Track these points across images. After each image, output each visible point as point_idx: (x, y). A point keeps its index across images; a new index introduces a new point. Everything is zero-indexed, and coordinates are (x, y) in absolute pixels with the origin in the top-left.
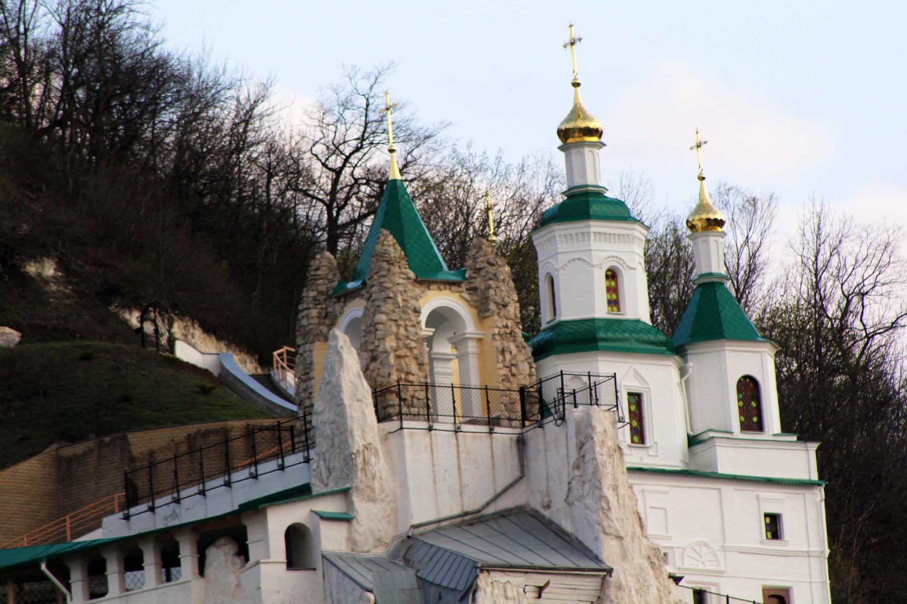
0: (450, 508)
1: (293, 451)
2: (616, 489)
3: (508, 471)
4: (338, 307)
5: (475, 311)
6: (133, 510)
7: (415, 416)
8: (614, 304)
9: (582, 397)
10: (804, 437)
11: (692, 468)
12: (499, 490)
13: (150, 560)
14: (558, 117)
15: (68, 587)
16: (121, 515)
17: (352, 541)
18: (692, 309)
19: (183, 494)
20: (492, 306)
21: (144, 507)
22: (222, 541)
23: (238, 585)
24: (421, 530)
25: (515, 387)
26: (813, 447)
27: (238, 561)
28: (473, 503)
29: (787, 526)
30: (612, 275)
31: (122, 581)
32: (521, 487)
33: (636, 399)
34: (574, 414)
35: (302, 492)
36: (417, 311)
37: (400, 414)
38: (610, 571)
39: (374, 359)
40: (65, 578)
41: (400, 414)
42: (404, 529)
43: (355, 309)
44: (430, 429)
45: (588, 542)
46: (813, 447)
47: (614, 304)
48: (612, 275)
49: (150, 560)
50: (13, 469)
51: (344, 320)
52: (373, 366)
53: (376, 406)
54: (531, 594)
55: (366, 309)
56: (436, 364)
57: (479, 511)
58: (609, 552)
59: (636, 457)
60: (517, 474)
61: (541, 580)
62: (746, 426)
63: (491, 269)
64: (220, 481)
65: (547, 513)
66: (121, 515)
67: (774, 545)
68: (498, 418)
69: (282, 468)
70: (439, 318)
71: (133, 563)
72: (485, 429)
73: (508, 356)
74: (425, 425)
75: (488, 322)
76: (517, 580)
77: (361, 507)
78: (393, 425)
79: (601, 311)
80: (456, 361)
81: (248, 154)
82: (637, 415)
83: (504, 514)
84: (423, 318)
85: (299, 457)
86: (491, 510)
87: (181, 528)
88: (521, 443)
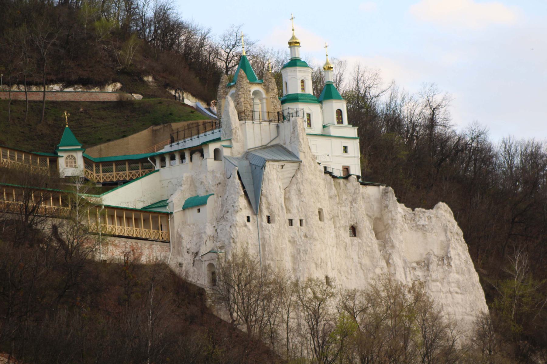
0: (258, 144)
1: (216, 128)
2: (303, 139)
3: (274, 134)
4: (228, 90)
5: (265, 91)
6: (173, 144)
7: (249, 119)
8: (303, 89)
9: (294, 115)
10: (354, 125)
12: (272, 139)
13: (177, 157)
14: (288, 39)
15: (155, 164)
17: (232, 153)
18: (324, 91)
19: (186, 140)
20: (270, 90)
21: (175, 143)
22: (197, 153)
24: (251, 150)
26: (356, 128)
27: (201, 158)
28: (265, 143)
29: (349, 149)
30: (303, 82)
31: (170, 163)
32: (278, 139)
33: (309, 115)
35: (218, 140)
36: (250, 91)
38: (301, 161)
39: (238, 104)
40: (154, 162)
41: (245, 119)
42: (246, 150)
43: (233, 90)
44: (253, 123)
46: (356, 128)
47: (303, 89)
48: (303, 82)
49: (177, 157)
51: (230, 93)
52: (237, 106)
53: (238, 116)
54: (280, 167)
55: (236, 90)
57: (266, 145)
58: (301, 156)
59: (309, 131)
60: (276, 135)
61: (283, 164)
62: (338, 123)
65: (284, 146)
66: (169, 145)
67: (346, 154)
68: (272, 120)
69: (213, 133)
70: (256, 93)
71: (173, 158)
73: (274, 103)
74: (252, 122)
75: (269, 94)
76: (276, 164)
77: (234, 144)
79: (300, 91)
82: (309, 119)
83: (273, 146)
84: (251, 93)
85: (218, 130)
86: (269, 145)
87: (175, 151)
88: (278, 127)
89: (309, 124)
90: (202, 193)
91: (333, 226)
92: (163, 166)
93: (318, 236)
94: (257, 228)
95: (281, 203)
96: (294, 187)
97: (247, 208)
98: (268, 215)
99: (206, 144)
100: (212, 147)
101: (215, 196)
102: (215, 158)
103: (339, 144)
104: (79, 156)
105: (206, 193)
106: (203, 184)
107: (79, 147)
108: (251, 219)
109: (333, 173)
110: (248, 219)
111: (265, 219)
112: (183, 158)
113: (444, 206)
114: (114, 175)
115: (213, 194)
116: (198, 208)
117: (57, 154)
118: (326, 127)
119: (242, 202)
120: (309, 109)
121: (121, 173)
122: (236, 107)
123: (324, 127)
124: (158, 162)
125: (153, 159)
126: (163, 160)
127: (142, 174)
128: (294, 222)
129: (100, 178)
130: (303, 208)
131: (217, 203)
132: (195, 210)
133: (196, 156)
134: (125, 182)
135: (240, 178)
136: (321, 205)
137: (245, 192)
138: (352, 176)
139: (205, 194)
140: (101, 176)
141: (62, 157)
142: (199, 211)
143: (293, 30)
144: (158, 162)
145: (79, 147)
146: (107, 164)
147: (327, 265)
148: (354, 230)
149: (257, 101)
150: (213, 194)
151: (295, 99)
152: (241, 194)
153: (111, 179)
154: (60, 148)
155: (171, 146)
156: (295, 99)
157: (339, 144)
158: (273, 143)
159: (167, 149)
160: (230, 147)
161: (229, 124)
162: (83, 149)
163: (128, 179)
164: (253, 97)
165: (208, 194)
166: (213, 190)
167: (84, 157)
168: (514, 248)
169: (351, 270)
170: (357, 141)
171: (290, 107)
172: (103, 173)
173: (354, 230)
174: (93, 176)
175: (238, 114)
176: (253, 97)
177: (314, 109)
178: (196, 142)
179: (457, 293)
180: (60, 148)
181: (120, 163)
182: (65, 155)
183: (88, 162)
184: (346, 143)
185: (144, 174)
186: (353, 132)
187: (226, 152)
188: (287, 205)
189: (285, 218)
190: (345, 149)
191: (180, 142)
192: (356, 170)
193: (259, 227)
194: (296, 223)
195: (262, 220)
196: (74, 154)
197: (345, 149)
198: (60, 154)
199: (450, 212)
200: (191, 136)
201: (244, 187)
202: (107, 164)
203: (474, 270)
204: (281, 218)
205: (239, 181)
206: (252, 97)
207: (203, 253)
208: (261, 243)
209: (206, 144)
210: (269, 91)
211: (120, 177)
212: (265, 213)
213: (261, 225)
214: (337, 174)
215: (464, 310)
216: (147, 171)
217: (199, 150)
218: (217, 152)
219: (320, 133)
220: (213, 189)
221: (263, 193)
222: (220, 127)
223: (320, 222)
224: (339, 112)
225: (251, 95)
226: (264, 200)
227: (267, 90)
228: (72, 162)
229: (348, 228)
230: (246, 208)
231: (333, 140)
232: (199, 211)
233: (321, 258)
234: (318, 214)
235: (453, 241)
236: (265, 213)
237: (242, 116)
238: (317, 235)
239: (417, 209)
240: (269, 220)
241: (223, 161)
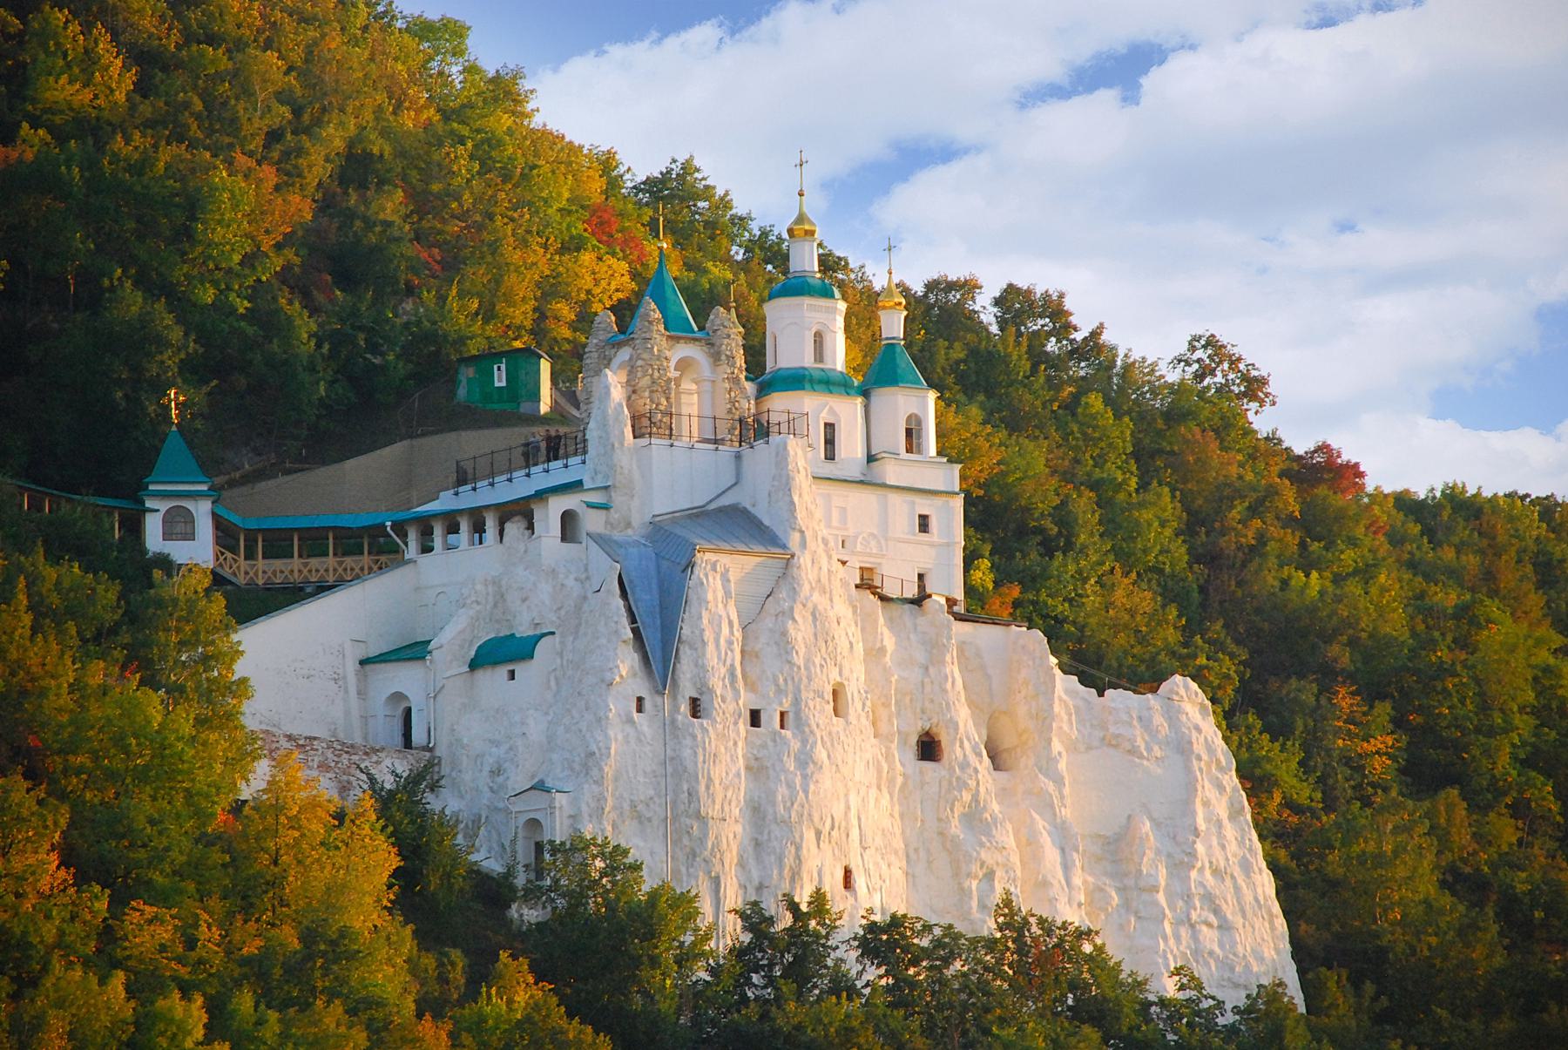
1: (575, 454)
4: (613, 351)
5: (711, 360)
6: (461, 489)
7: (660, 436)
9: (784, 428)
11: (868, 479)
13: (464, 526)
15: (407, 545)
16: (452, 491)
19: (497, 479)
20: (723, 357)
21: (469, 487)
22: (516, 518)
23: (526, 551)
25: (737, 417)
27: (527, 533)
29: (934, 523)
31: (445, 541)
33: (830, 428)
34: (774, 438)
35: (575, 486)
37: (650, 434)
38: (793, 556)
39: (634, 392)
41: (650, 434)
43: (624, 354)
45: (780, 534)
46: (751, 935)
49: (464, 526)
50: (378, 452)
51: (616, 362)
52: (633, 397)
53: (633, 426)
55: (631, 356)
56: (683, 396)
58: (794, 541)
59: (829, 469)
62: (909, 450)
63: (726, 331)
64: (523, 472)
66: (452, 491)
68: (723, 440)
70: (683, 365)
71: (453, 529)
72: (712, 446)
74: (668, 442)
75: (721, 369)
78: (644, 441)
79: (808, 361)
80: (696, 396)
81: (300, 369)
82: (830, 442)
83: (720, 510)
84: (672, 364)
85: (578, 459)
86: (713, 506)
87: (461, 512)
88: (738, 457)
89: (830, 456)
90: (523, 630)
91: (871, 731)
92: (426, 549)
93: (829, 756)
94: (661, 731)
95: (732, 665)
96: (769, 622)
97: (640, 674)
98: (695, 695)
99: (541, 495)
100: (557, 506)
101: (557, 638)
102: (565, 537)
103: (903, 511)
104: (202, 511)
105: (535, 629)
106: (527, 603)
107: (204, 488)
108: (647, 705)
109: (882, 588)
110: (640, 700)
111: (684, 708)
112: (479, 528)
113: (1187, 688)
114: (292, 568)
115: (553, 633)
116: (511, 668)
117: (143, 503)
118: (877, 460)
119: (626, 662)
120: (832, 411)
121: (314, 562)
122: (629, 398)
123: (871, 458)
124: (413, 536)
125: (400, 528)
126: (426, 533)
127: (370, 569)
128: (764, 717)
129: (256, 574)
130: (790, 682)
131: (562, 658)
132: (502, 671)
133: (514, 528)
134: (323, 588)
135: (624, 594)
136: (841, 674)
137: (636, 632)
138: (934, 597)
139: (530, 633)
140: (262, 570)
141: (158, 510)
142: (512, 675)
143: (801, 195)
144: (413, 536)
145: (204, 488)
146: (277, 544)
147: (848, 835)
148: (928, 748)
149: (687, 385)
150: (553, 633)
151: (796, 380)
152: (625, 638)
153: (322, 575)
154: (151, 487)
155: (457, 494)
156: (796, 380)
157: (903, 511)
158: (726, 501)
159: (445, 502)
160: (605, 507)
161: (609, 449)
162: (216, 494)
163: (331, 579)
164: (677, 374)
165: (538, 632)
166: (552, 622)
167: (214, 515)
168: (1237, 872)
169: (916, 850)
170: (958, 503)
171: (780, 404)
172: (264, 558)
173: (928, 748)
174: (238, 568)
175: (633, 418)
176: (677, 374)
177: (847, 412)
178: (520, 486)
179: (1209, 925)
180: (151, 487)
181: (314, 541)
182: (163, 506)
183: (225, 534)
184: (924, 506)
185: (375, 568)
186: (948, 477)
187: (592, 522)
188: (748, 669)
189: (741, 702)
190: (924, 523)
191: (479, 485)
192: (949, 583)
193: (670, 729)
194: (771, 720)
195: (676, 709)
196: (189, 504)
197: (924, 523)
198: (149, 504)
199: (1202, 705)
200: (510, 471)
201: (633, 620)
202: (277, 544)
203: (1264, 865)
204: (729, 705)
205: (621, 603)
206: (673, 374)
207: (514, 789)
208: (670, 769)
209: (541, 495)
210: (719, 360)
211: (310, 571)
212: (688, 690)
213: (673, 721)
214: (891, 590)
215: (1227, 975)
216: (383, 558)
217: (522, 511)
218: (569, 521)
219: (857, 475)
220: (549, 623)
221: (684, 638)
222: (585, 452)
223: (835, 719)
224: (912, 436)
225: (672, 369)
226: (686, 654)
227: (716, 357)
228: (180, 525)
229: (914, 739)
230: (635, 675)
231: (895, 499)
232: (512, 675)
233: (833, 818)
234: (831, 699)
235: (1207, 790)
236: (688, 690)
237: (642, 426)
238: (824, 755)
239: (1109, 693)
240: (696, 708)
241: (584, 544)
